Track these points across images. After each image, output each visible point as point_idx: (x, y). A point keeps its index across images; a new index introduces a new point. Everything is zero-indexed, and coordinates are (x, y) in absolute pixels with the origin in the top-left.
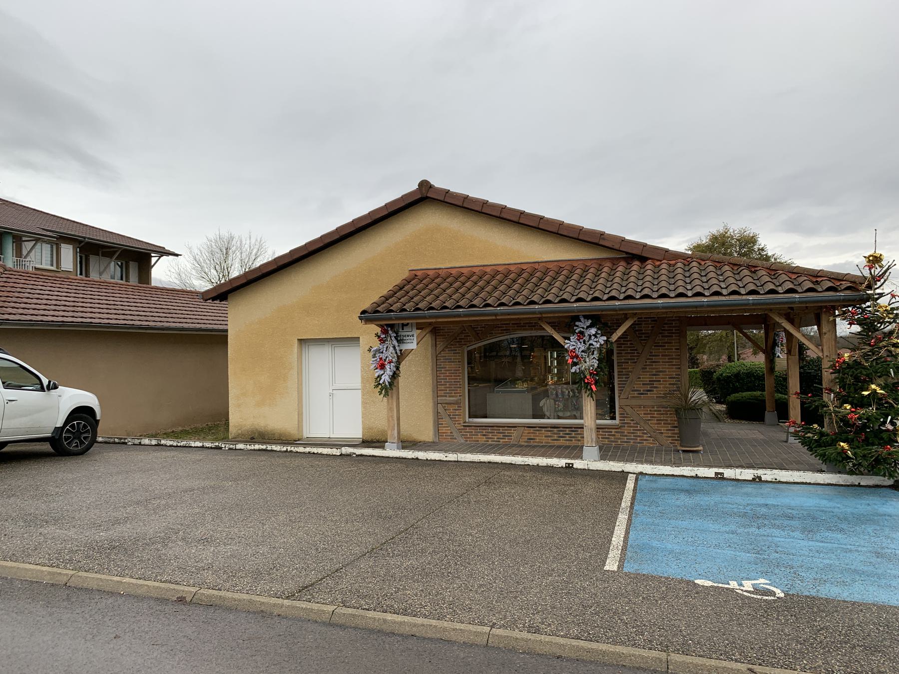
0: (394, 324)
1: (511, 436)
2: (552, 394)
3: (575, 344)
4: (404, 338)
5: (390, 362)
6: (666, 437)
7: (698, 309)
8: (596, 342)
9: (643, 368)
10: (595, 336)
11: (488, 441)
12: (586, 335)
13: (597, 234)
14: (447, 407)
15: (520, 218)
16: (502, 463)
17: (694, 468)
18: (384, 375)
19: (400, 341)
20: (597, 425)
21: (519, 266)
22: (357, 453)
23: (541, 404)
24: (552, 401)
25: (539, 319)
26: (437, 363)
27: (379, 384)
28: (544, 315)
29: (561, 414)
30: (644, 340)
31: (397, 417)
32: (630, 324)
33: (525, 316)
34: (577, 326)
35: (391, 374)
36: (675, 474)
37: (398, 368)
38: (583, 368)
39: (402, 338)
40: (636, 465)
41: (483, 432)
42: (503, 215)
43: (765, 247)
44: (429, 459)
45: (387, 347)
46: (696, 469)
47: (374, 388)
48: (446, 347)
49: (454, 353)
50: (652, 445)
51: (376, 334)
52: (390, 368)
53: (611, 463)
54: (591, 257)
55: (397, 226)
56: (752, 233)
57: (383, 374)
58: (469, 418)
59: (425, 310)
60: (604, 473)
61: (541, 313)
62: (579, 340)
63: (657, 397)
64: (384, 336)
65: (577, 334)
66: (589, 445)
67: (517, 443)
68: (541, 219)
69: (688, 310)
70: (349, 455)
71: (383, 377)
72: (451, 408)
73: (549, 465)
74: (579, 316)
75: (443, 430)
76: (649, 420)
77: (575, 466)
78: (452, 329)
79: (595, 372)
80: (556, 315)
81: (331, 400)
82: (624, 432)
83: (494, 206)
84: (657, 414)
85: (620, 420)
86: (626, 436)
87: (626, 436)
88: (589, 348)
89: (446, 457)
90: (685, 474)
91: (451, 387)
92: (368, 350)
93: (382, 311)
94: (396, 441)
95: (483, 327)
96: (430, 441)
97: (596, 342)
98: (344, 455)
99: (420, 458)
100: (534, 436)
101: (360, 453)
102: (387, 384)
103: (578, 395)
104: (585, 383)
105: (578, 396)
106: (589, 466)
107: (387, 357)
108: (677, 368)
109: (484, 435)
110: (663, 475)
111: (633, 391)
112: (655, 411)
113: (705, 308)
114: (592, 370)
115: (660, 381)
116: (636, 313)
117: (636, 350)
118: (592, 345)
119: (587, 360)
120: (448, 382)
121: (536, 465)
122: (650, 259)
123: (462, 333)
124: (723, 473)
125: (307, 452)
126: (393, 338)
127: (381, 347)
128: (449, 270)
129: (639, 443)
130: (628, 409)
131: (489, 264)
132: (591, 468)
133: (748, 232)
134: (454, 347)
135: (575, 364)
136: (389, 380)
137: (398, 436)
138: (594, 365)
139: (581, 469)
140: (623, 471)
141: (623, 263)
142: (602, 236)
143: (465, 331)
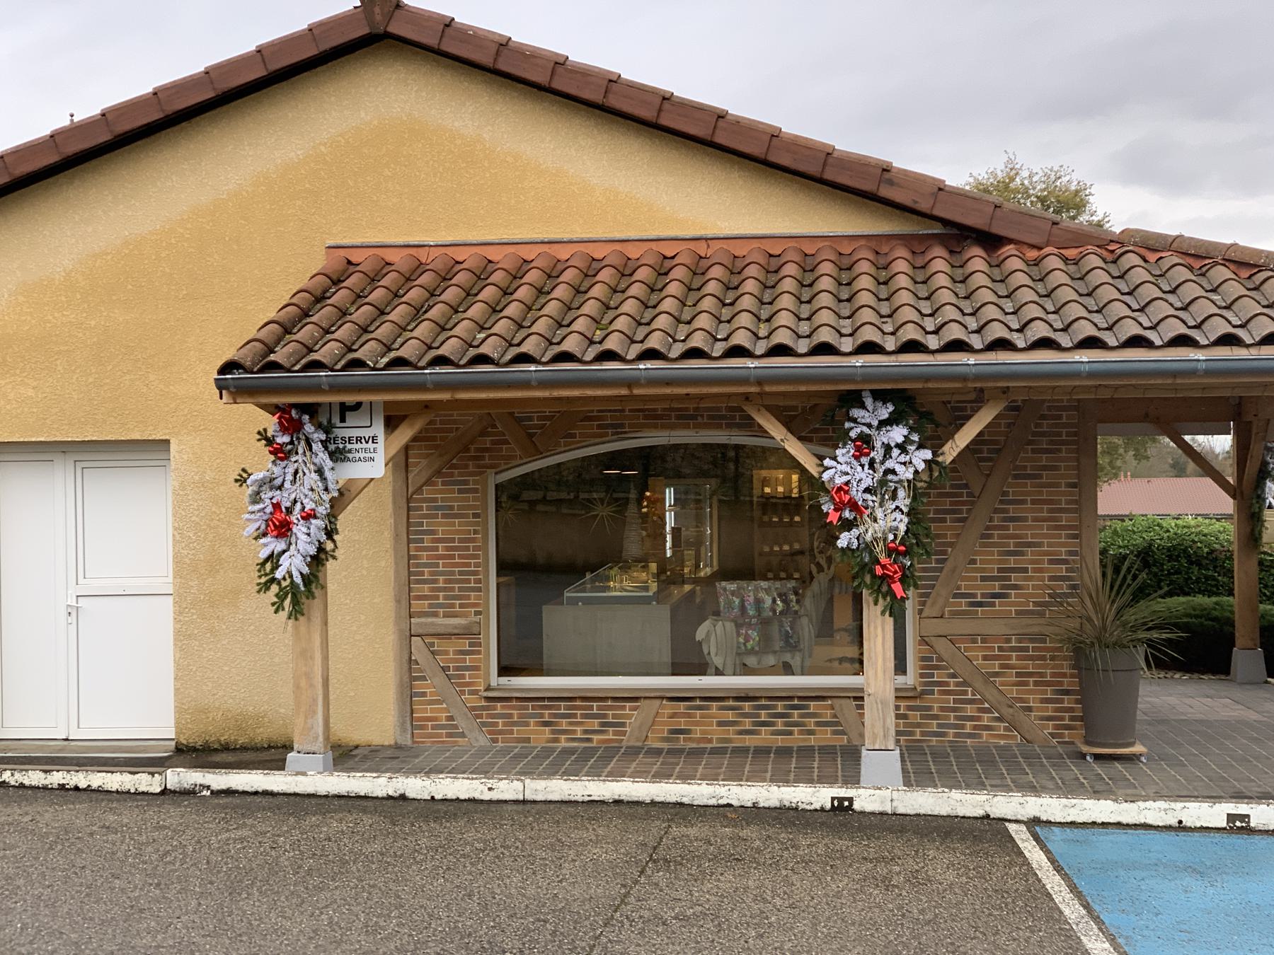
0: (318, 405)
1: (623, 725)
2: (730, 605)
3: (848, 469)
4: (349, 446)
5: (308, 517)
6: (1042, 718)
7: (1179, 381)
8: (904, 464)
9: (983, 536)
10: (902, 448)
11: (556, 740)
12: (878, 445)
13: (874, 167)
14: (438, 644)
15: (660, 110)
16: (653, 803)
17: (1173, 805)
18: (287, 554)
19: (338, 455)
20: (897, 690)
21: (653, 245)
22: (215, 787)
23: (700, 634)
24: (730, 626)
25: (747, 399)
26: (408, 518)
27: (273, 580)
28: (767, 389)
29: (751, 661)
30: (990, 459)
31: (322, 675)
32: (996, 413)
33: (715, 390)
34: (855, 420)
35: (312, 550)
36: (1125, 822)
37: (330, 533)
38: (868, 537)
39: (341, 446)
40: (1022, 800)
41: (542, 716)
42: (614, 102)
43: (1106, 219)
44: (438, 797)
45: (296, 472)
46: (1179, 805)
47: (259, 592)
48: (438, 473)
49: (460, 491)
50: (1002, 742)
51: (259, 433)
52: (309, 535)
53: (956, 794)
54: (840, 230)
55: (290, 115)
56: (1076, 183)
57: (284, 552)
58: (500, 675)
59: (296, 368)
60: (941, 821)
61: (760, 382)
62: (857, 458)
63: (1018, 612)
64: (286, 439)
65: (854, 441)
66: (877, 748)
67: (639, 744)
68: (719, 117)
69: (1152, 382)
70: (189, 793)
71: (285, 561)
72: (451, 647)
73: (787, 804)
74: (861, 390)
75: (425, 711)
76: (997, 674)
77: (857, 806)
78: (455, 422)
79: (902, 548)
80: (803, 388)
81: (73, 628)
82: (930, 708)
83: (585, 74)
84: (1018, 658)
85: (922, 676)
86: (936, 717)
87: (936, 717)
88: (883, 482)
89: (490, 789)
90: (1150, 821)
91: (452, 589)
92: (236, 481)
93: (287, 365)
94: (319, 745)
95: (545, 418)
96: (386, 743)
97: (904, 464)
98: (174, 792)
99: (411, 794)
100: (686, 723)
101: (224, 787)
102: (298, 580)
103: (796, 608)
104: (874, 576)
105: (796, 612)
106: (895, 804)
107: (295, 501)
108: (1069, 536)
109: (546, 724)
110: (1094, 823)
111: (956, 596)
112: (1013, 649)
113: (1200, 376)
114: (893, 541)
115: (1026, 570)
116: (1008, 387)
117: (966, 486)
118: (893, 472)
119: (879, 513)
120: (442, 573)
121: (750, 804)
122: (1010, 241)
123: (483, 433)
124: (1248, 816)
125: (55, 786)
126: (317, 447)
127: (277, 470)
128: (449, 251)
129: (970, 736)
130: (942, 646)
131: (566, 237)
132: (901, 810)
133: (1065, 179)
134: (461, 475)
135: (848, 525)
136: (306, 570)
137: (324, 733)
138: (897, 529)
139: (873, 813)
140: (988, 816)
141: (938, 251)
142: (887, 175)
143: (494, 426)
